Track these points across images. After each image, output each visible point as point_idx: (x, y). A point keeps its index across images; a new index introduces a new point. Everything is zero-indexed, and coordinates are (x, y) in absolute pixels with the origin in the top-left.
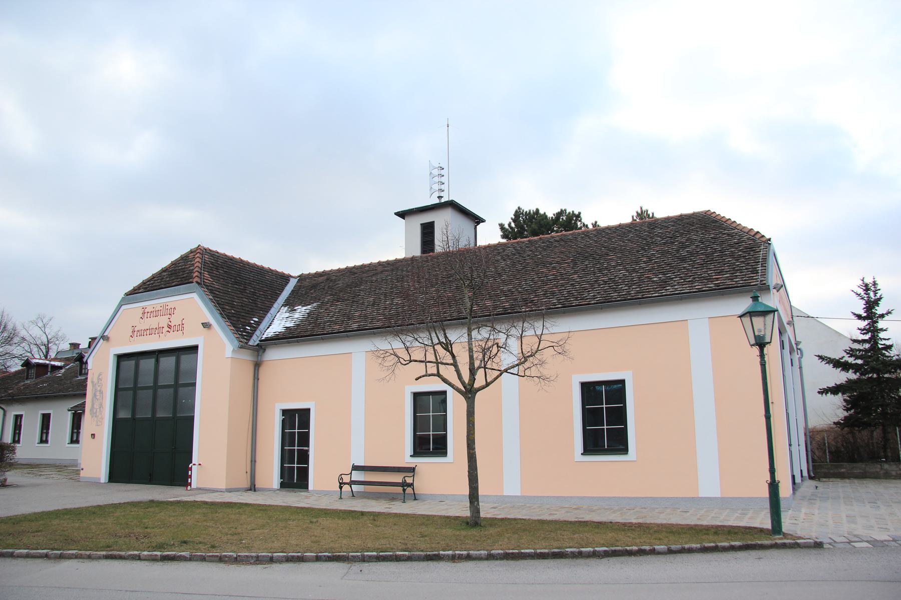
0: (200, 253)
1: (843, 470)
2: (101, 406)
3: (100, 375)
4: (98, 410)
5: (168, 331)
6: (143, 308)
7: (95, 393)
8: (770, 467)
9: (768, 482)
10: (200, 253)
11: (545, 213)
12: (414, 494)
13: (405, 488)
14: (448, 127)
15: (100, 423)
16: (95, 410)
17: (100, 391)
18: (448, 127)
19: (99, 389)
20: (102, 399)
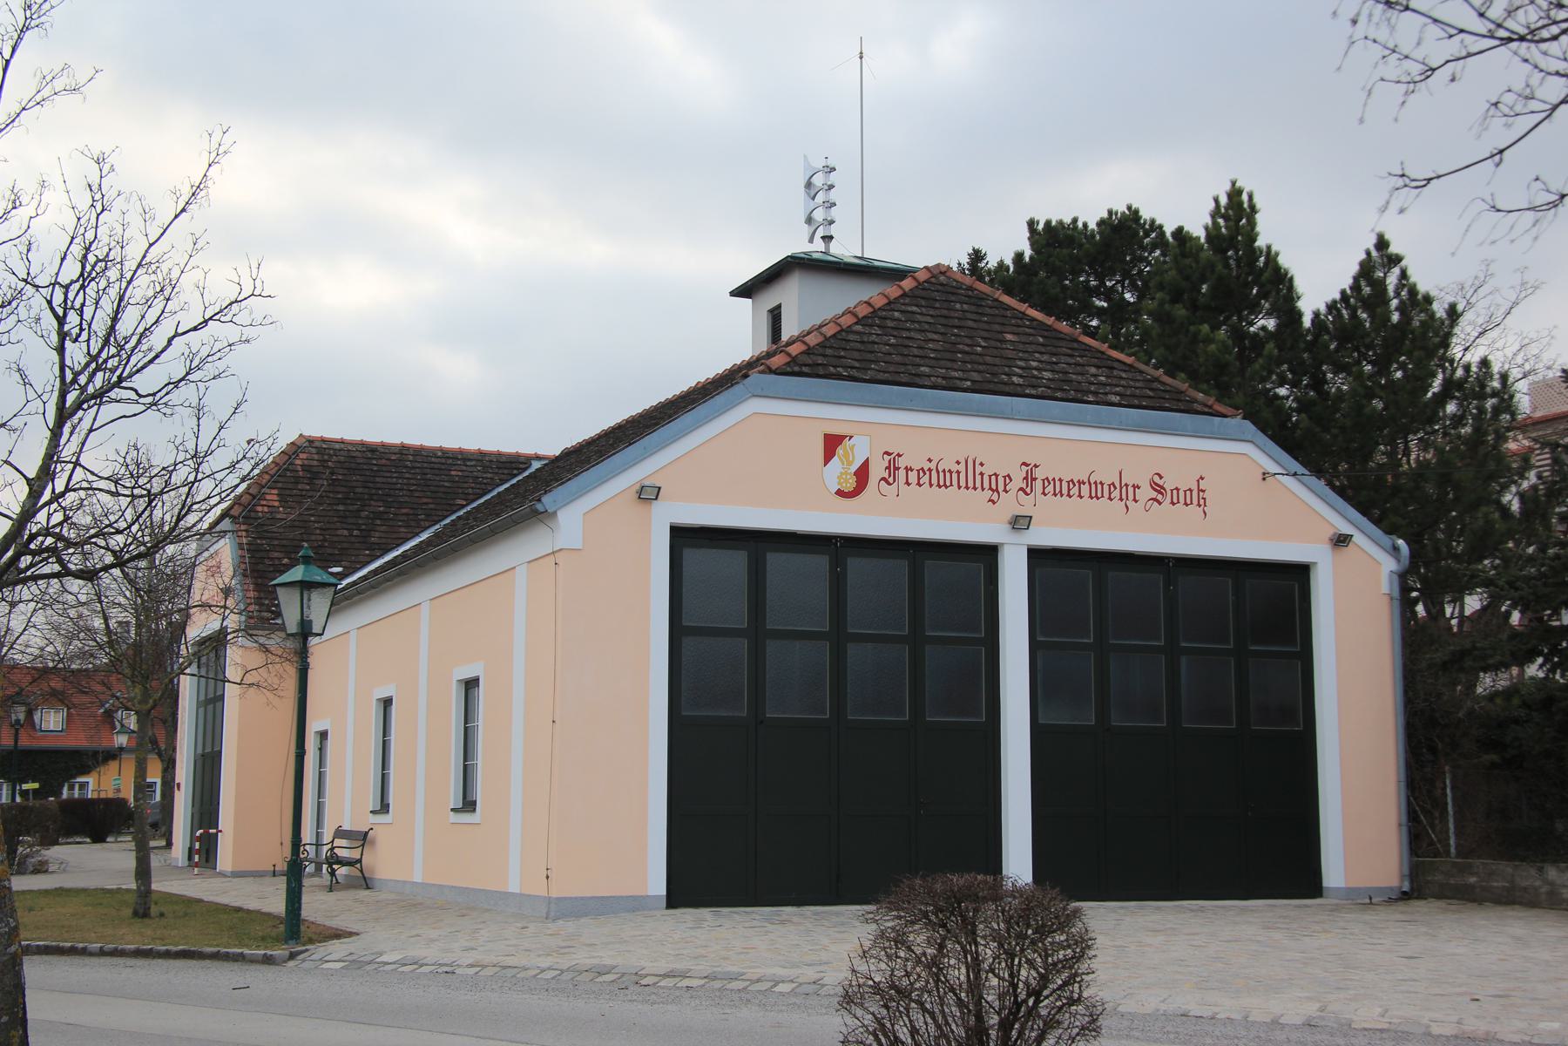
1: (1473, 880)
5: (1155, 500)
8: (293, 835)
9: (288, 860)
11: (1129, 208)
12: (365, 878)
13: (335, 867)
14: (861, 58)
18: (861, 58)
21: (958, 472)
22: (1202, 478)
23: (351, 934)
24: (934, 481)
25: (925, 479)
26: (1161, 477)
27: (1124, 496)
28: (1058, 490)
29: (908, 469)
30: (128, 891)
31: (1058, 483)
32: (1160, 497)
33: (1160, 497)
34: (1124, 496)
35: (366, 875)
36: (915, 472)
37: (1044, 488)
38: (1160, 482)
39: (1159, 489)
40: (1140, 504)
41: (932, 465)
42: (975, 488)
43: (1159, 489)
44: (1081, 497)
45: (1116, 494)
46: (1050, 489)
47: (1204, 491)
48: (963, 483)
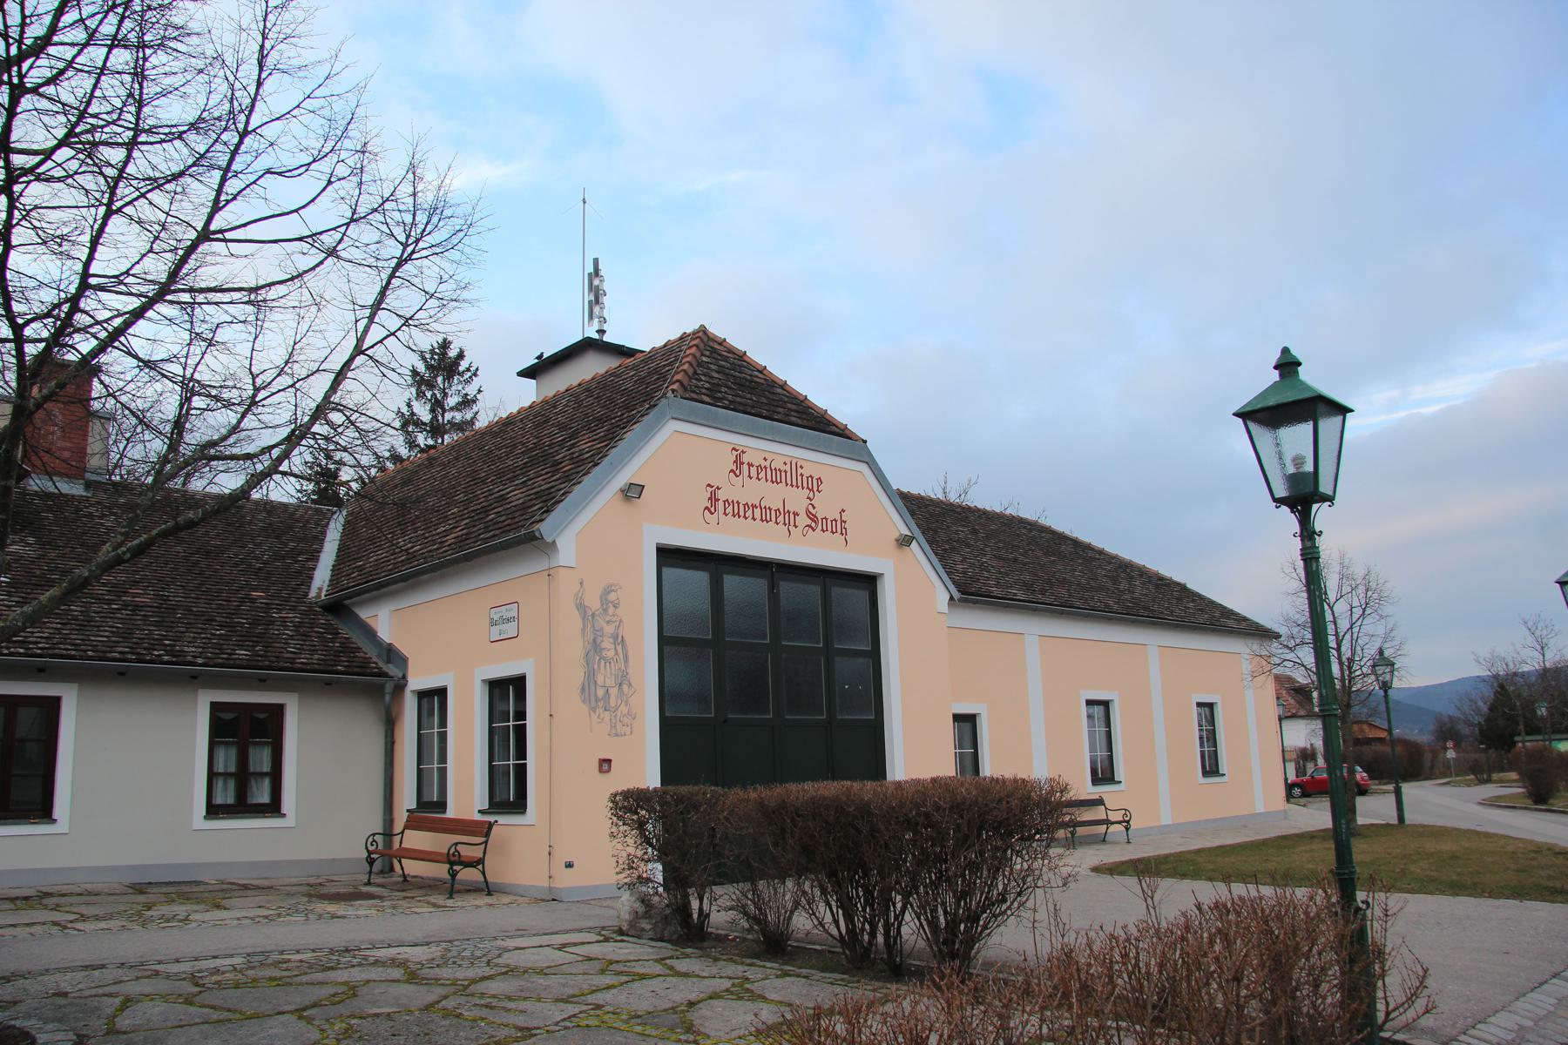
0: (702, 340)
2: (623, 680)
3: (609, 590)
4: (614, 692)
5: (809, 526)
6: (734, 449)
7: (594, 640)
10: (702, 340)
13: (457, 868)
14: (585, 202)
15: (627, 730)
16: (601, 692)
17: (615, 637)
19: (609, 629)
20: (626, 660)
21: (786, 472)
22: (843, 511)
23: (20, 1002)
24: (769, 477)
25: (762, 475)
26: (814, 508)
27: (787, 522)
28: (736, 512)
29: (750, 465)
30: (1310, 836)
31: (736, 505)
32: (813, 524)
33: (813, 524)
34: (787, 522)
35: (489, 880)
36: (755, 468)
37: (725, 509)
38: (814, 512)
39: (813, 518)
40: (800, 528)
41: (768, 464)
42: (798, 487)
43: (813, 518)
44: (755, 520)
45: (781, 519)
46: (729, 510)
47: (845, 522)
48: (789, 482)
